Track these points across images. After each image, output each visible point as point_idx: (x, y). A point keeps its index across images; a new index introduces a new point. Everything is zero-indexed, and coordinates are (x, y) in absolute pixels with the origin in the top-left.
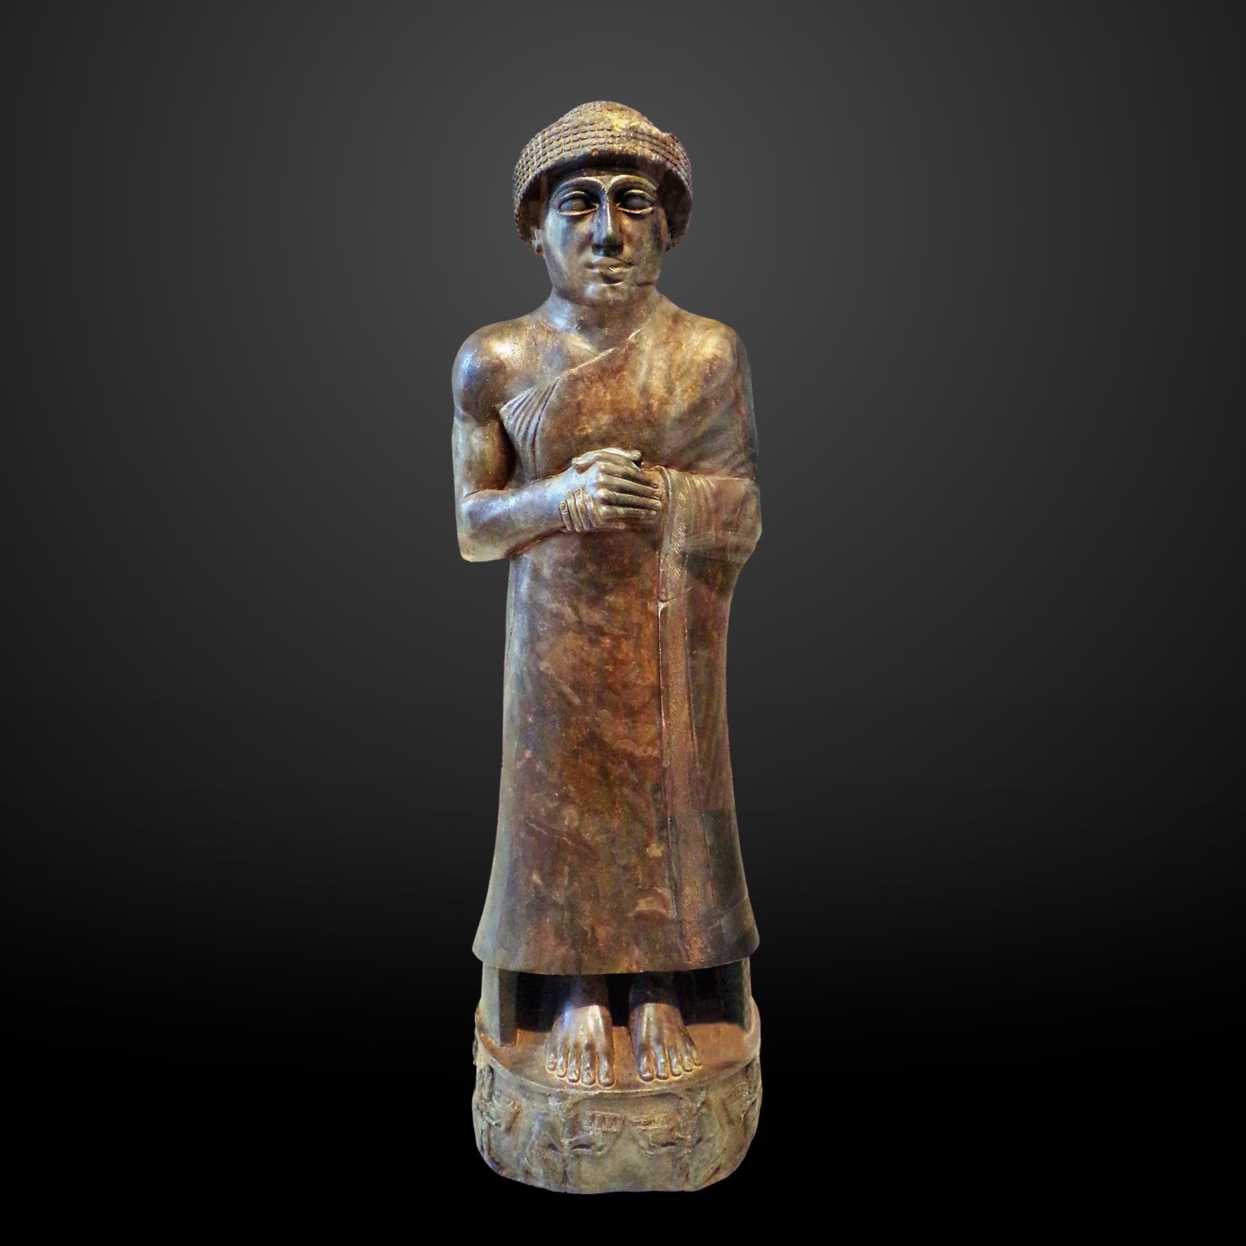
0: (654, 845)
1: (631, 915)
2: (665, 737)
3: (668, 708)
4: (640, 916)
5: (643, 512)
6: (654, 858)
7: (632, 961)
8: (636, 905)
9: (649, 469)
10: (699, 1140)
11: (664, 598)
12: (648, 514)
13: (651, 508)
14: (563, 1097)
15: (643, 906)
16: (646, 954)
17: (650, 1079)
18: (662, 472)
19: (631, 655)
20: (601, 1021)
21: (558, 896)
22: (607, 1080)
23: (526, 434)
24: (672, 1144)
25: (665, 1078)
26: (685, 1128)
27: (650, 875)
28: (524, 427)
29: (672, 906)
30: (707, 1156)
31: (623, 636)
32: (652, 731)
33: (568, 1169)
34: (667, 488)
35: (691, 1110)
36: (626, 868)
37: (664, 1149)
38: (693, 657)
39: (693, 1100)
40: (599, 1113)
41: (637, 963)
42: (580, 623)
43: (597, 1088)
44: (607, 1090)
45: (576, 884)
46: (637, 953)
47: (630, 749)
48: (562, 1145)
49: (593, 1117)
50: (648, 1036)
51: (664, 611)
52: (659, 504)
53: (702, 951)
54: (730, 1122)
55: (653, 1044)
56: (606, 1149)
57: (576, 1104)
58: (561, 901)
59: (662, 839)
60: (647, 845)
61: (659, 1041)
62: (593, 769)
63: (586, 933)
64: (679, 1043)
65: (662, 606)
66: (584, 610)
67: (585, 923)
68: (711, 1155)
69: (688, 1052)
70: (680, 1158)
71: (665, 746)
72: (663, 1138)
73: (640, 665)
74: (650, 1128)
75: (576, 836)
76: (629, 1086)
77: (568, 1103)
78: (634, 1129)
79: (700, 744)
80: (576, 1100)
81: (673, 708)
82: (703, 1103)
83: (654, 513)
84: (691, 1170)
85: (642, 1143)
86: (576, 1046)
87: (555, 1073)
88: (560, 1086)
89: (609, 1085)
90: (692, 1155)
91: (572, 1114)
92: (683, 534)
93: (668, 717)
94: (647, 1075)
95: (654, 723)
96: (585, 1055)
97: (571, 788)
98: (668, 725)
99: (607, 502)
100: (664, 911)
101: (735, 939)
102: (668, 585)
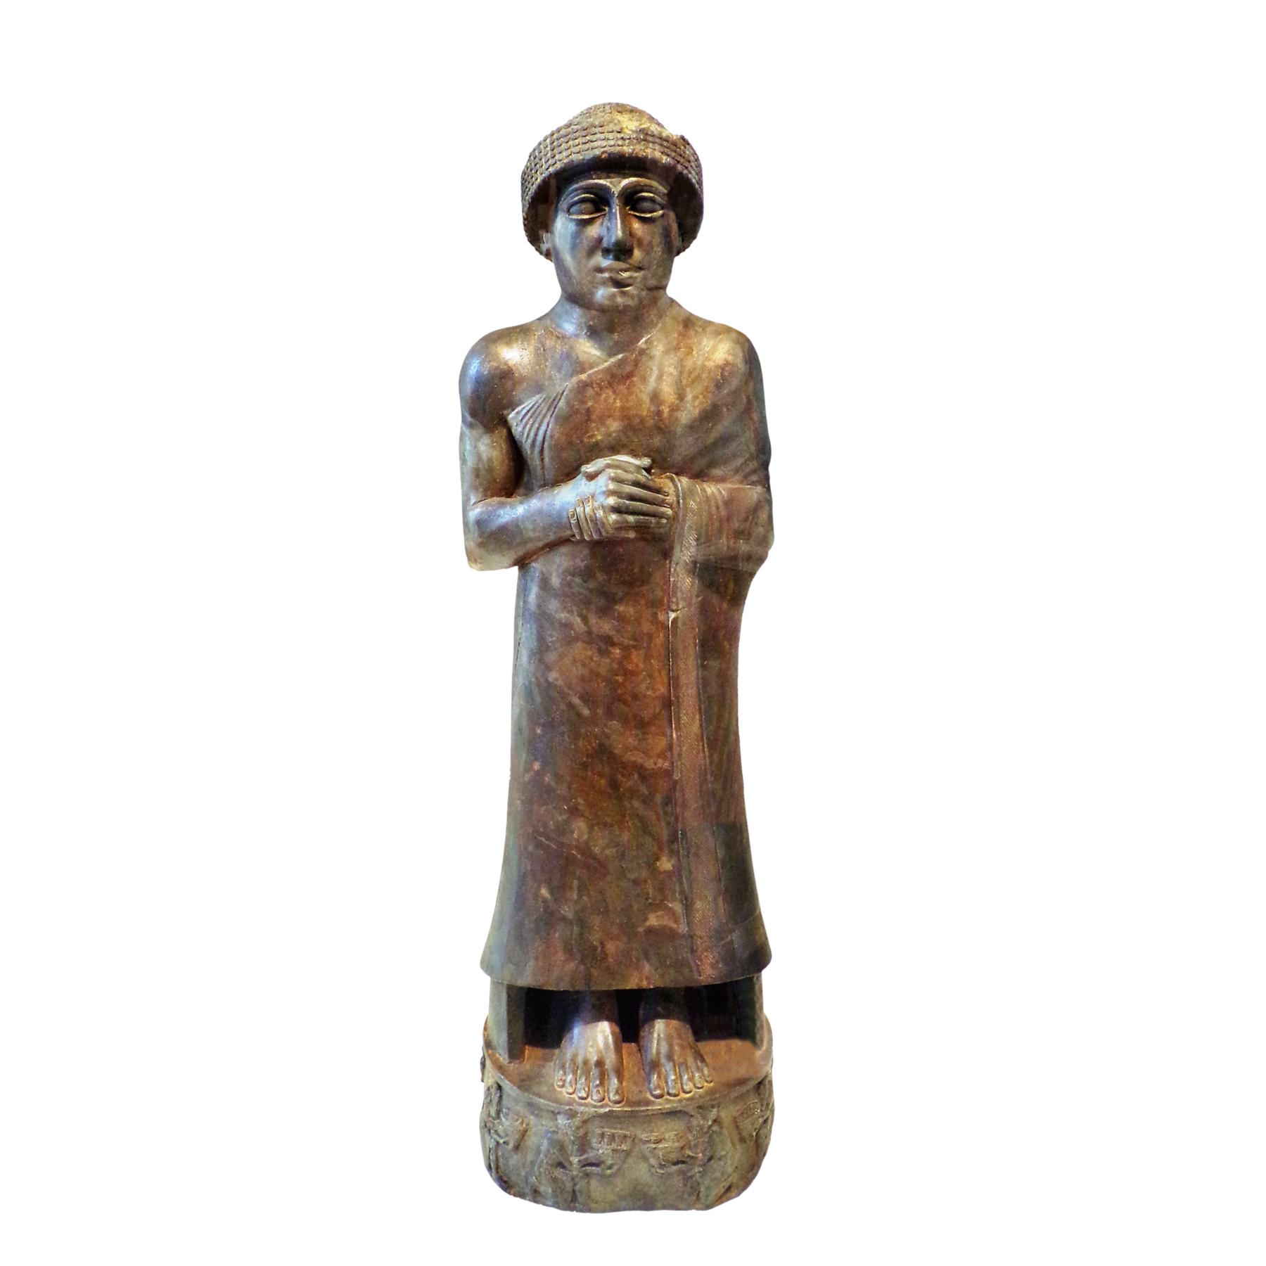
0: (664, 859)
1: (641, 929)
2: (676, 749)
3: (678, 719)
4: (650, 931)
5: (653, 520)
6: (665, 872)
7: (643, 977)
8: (646, 919)
9: (659, 476)
10: (710, 1159)
11: (674, 607)
12: (658, 523)
13: (661, 516)
14: (572, 1115)
15: (653, 920)
16: (656, 969)
17: (661, 1096)
18: (672, 480)
19: (642, 666)
20: (610, 1038)
21: (567, 911)
22: (617, 1097)
23: (534, 441)
24: (683, 1162)
25: (676, 1095)
26: (696, 1146)
27: (661, 890)
28: (532, 434)
29: (683, 920)
30: (718, 1174)
31: (633, 647)
32: (662, 743)
33: (577, 1188)
34: (678, 496)
35: (702, 1128)
36: (636, 882)
37: (675, 1168)
39: (704, 1118)
40: (608, 1131)
41: (647, 978)
42: (589, 633)
43: (607, 1105)
44: (617, 1108)
45: (585, 898)
46: (647, 968)
47: (640, 761)
48: (571, 1163)
49: (602, 1135)
50: (658, 1053)
51: (675, 621)
52: (670, 512)
53: (713, 966)
54: (742, 1140)
55: (663, 1060)
56: (615, 1167)
57: (585, 1122)
58: (570, 915)
59: (673, 853)
60: (658, 859)
61: (670, 1058)
62: (603, 781)
63: (595, 948)
64: (690, 1060)
65: (672, 615)
67: (595, 938)
68: (723, 1174)
69: (699, 1069)
70: (691, 1177)
71: (676, 758)
72: (673, 1156)
73: (650, 676)
74: (661, 1146)
75: (585, 849)
76: (639, 1103)
77: (577, 1121)
78: (644, 1147)
79: (711, 756)
81: (684, 719)
82: (715, 1121)
83: (664, 521)
84: (702, 1189)
85: (653, 1161)
86: (586, 1062)
87: (564, 1090)
88: (569, 1104)
89: (618, 1102)
90: (703, 1174)
91: (582, 1132)
92: (694, 543)
94: (658, 1092)
95: (664, 734)
96: (595, 1072)
97: (580, 801)
98: (679, 737)
99: (616, 510)
100: (675, 926)
101: (746, 954)
102: (679, 594)
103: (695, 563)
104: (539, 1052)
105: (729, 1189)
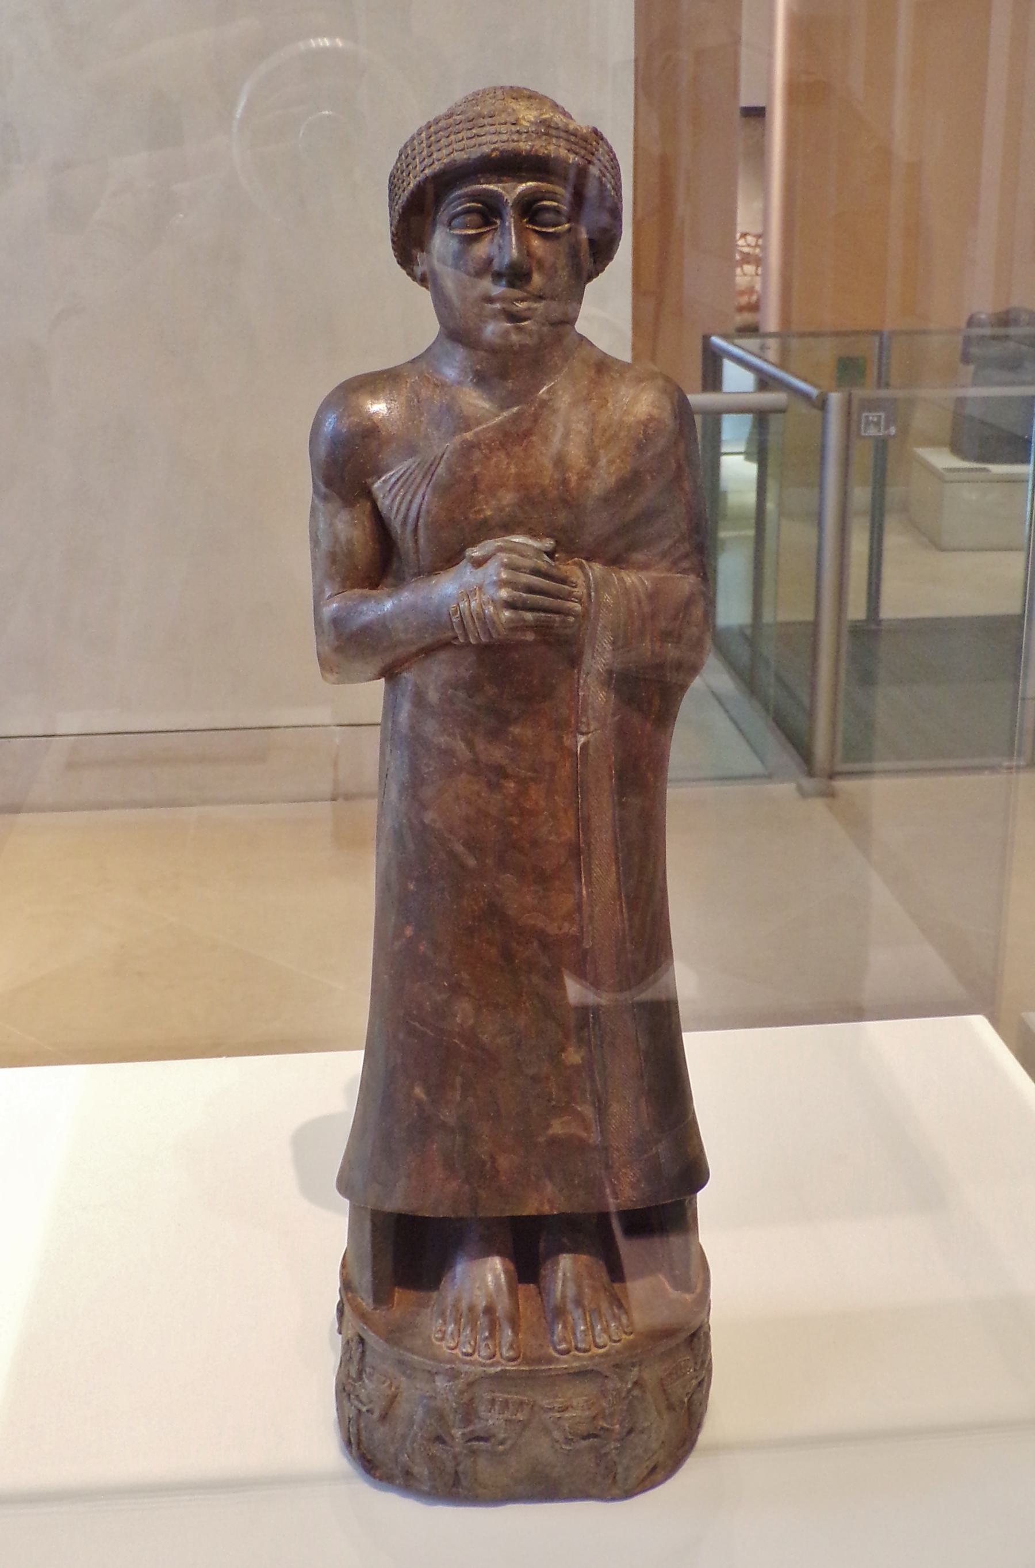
1: (541, 1139)
4: (554, 1142)
6: (572, 1066)
7: (544, 1200)
8: (548, 1126)
10: (630, 1431)
11: (584, 729)
12: (563, 621)
13: (568, 613)
14: (454, 1375)
15: (557, 1128)
16: (561, 1190)
17: (567, 1352)
19: (542, 803)
21: (448, 1116)
22: (511, 1353)
24: (595, 1436)
25: (585, 1351)
26: (612, 1415)
29: (595, 1128)
30: (640, 1451)
31: (532, 779)
32: (568, 902)
33: (461, 1468)
34: (588, 587)
35: (619, 1393)
36: (535, 1079)
37: (585, 1443)
38: (622, 805)
39: (622, 1379)
40: (500, 1396)
42: (476, 761)
43: (498, 1363)
44: (511, 1367)
45: (471, 1100)
46: (549, 1188)
47: (541, 925)
48: (453, 1437)
49: (493, 1401)
50: (564, 1296)
51: (585, 746)
53: (633, 1186)
55: (570, 1306)
56: (509, 1442)
57: (470, 1385)
59: (582, 1042)
60: (563, 1050)
62: (494, 951)
64: (604, 1306)
65: (582, 739)
66: (481, 745)
67: (483, 1150)
68: (646, 1451)
69: (615, 1317)
70: (606, 1454)
72: (583, 1429)
74: (567, 1415)
76: (539, 1361)
77: (460, 1383)
79: (631, 919)
80: (471, 1379)
81: (597, 872)
82: (636, 1383)
83: (572, 619)
84: (620, 1470)
85: (557, 1435)
86: (471, 1309)
87: (443, 1344)
90: (621, 1451)
91: (466, 1397)
92: (609, 647)
93: (589, 883)
96: (483, 1321)
97: (465, 975)
98: (590, 894)
100: (584, 1135)
102: (590, 712)
103: (610, 672)
104: (412, 1295)
105: (653, 1470)
